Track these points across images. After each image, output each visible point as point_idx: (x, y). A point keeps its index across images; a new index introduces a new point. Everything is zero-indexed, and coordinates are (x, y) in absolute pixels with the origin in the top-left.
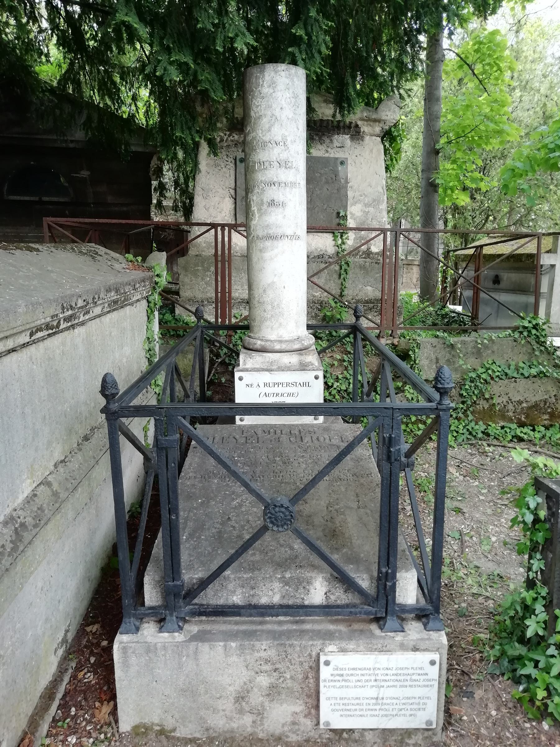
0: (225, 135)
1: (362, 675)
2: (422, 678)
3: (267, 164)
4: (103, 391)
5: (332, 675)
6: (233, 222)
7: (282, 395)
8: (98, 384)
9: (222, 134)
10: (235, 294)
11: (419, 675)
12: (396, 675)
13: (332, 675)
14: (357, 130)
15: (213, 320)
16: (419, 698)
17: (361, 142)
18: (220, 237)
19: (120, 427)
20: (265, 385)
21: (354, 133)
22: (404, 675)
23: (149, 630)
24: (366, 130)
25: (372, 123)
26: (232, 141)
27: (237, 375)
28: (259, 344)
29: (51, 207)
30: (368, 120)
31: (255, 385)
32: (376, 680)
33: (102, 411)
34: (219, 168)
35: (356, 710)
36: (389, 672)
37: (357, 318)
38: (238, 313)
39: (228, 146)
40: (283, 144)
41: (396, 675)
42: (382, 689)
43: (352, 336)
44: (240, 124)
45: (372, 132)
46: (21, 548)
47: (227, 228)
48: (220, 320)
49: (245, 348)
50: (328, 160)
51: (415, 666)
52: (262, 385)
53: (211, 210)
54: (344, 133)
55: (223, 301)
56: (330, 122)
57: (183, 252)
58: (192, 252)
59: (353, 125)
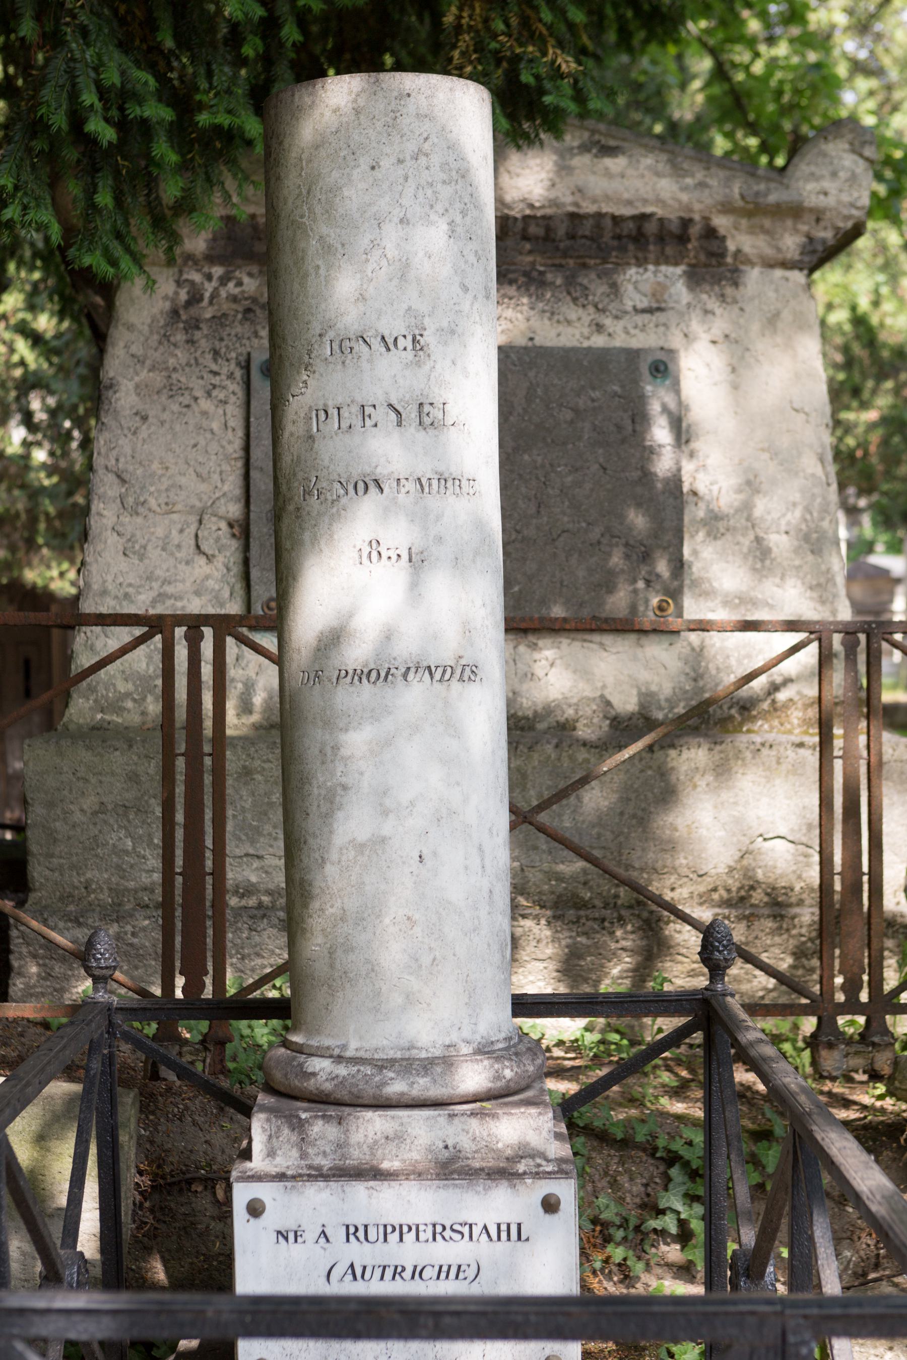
0: (209, 277)
3: (351, 415)
6: (234, 608)
7: (418, 1273)
9: (197, 277)
14: (714, 246)
17: (729, 291)
18: (181, 653)
20: (351, 1232)
21: (702, 257)
24: (747, 249)
25: (767, 223)
26: (234, 299)
27: (241, 1194)
30: (753, 211)
31: (311, 1234)
34: (186, 400)
38: (250, 963)
39: (220, 320)
40: (408, 343)
43: (698, 1037)
44: (262, 246)
45: (769, 251)
47: (208, 632)
48: (862, 739)
49: (271, 1089)
50: (600, 360)
53: (154, 553)
54: (663, 259)
55: (194, 911)
56: (608, 223)
58: (81, 709)
59: (695, 231)
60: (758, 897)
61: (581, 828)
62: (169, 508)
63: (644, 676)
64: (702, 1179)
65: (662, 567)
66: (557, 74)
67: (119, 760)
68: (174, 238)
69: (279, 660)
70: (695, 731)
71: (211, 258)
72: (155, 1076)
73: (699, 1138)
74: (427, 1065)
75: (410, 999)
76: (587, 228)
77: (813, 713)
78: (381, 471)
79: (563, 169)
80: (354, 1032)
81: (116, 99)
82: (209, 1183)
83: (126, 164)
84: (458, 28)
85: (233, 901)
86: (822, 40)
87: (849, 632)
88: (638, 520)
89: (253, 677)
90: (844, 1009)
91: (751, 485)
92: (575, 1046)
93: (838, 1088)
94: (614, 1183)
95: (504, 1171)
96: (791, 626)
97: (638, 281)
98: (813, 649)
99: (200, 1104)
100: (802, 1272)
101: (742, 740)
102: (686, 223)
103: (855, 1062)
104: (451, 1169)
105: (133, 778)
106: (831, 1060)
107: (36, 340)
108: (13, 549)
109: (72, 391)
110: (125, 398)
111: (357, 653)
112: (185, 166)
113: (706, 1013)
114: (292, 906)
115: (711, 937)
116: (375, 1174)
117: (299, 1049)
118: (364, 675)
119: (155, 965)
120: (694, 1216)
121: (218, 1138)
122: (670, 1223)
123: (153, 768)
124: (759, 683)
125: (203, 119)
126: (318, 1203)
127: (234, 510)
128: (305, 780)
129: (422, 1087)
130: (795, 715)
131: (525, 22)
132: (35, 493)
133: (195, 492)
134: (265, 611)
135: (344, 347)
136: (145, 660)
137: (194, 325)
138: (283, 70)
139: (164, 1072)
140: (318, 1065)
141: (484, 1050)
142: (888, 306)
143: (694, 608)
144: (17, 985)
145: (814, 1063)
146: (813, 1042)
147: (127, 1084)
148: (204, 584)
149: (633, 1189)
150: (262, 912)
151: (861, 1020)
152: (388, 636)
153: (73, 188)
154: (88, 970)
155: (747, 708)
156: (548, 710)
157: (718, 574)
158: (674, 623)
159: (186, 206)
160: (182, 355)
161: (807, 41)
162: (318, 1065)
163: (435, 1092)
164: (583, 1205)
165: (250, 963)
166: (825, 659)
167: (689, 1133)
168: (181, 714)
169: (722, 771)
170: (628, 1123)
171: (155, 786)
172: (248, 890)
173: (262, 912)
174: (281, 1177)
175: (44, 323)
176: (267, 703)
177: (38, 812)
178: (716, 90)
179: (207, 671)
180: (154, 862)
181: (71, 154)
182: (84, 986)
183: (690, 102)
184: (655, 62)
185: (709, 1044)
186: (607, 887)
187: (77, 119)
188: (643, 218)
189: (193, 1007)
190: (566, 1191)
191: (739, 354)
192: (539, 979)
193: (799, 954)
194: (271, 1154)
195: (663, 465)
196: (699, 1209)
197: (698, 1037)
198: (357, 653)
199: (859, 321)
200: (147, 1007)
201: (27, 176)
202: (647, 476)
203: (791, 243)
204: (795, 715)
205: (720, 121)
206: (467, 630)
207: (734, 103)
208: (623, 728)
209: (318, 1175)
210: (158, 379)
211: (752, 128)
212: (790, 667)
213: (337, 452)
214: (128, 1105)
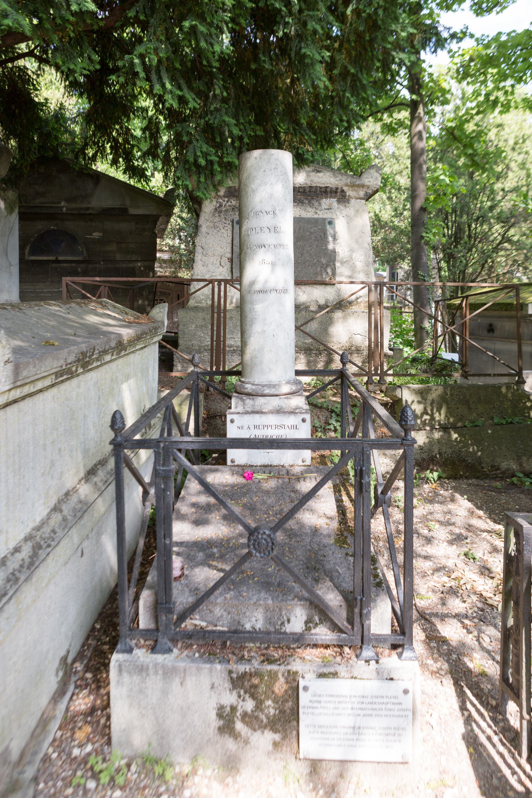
1: (339, 702)
2: (397, 707)
3: (258, 230)
4: (113, 426)
5: (310, 701)
6: (229, 278)
8: (108, 420)
10: (229, 342)
11: (393, 704)
12: (372, 703)
13: (310, 701)
15: (327, 491)
16: (395, 728)
18: (216, 289)
19: (125, 458)
20: (255, 427)
22: (379, 703)
23: (141, 655)
27: (229, 417)
28: (249, 387)
29: (65, 265)
30: (353, 186)
31: (246, 427)
32: (352, 709)
33: (111, 443)
35: (334, 739)
36: (365, 700)
37: (344, 364)
38: (232, 362)
39: (227, 211)
41: (372, 703)
42: (358, 718)
44: (236, 193)
46: (37, 564)
47: (223, 283)
49: (236, 392)
51: (389, 695)
52: (252, 427)
53: (210, 266)
54: (331, 197)
55: (218, 350)
57: (183, 305)
58: (192, 303)
59: (339, 190)
60: (353, 348)
61: (311, 332)
62: (214, 255)
63: (326, 295)
64: (341, 416)
65: (329, 271)
66: (308, 151)
67: (201, 315)
68: (218, 191)
69: (240, 290)
70: (339, 308)
71: (225, 196)
72: (208, 390)
73: (339, 406)
74: (274, 386)
75: (270, 370)
76: (313, 190)
77: (367, 304)
78: (265, 243)
79: (308, 176)
80: (255, 379)
81: (205, 155)
82: (221, 416)
83: (208, 171)
84: (285, 140)
85: (227, 349)
86: (368, 150)
87: (376, 284)
88: (324, 261)
89: (234, 295)
90: (374, 375)
91: (352, 250)
92: (309, 384)
93: (372, 395)
94: (318, 417)
95: (293, 412)
96: (362, 283)
97: (325, 202)
98: (367, 288)
99: (219, 397)
100: (366, 434)
101: (349, 311)
102: (337, 189)
103: (377, 388)
104: (279, 411)
105: (204, 319)
106: (371, 387)
107: (182, 219)
108: (176, 268)
109: (191, 230)
110: (204, 229)
111: (258, 287)
112: (221, 172)
113: (342, 375)
114: (242, 350)
115: (342, 357)
116: (262, 413)
117: (243, 382)
118: (260, 292)
119: (209, 364)
120: (337, 425)
121: (223, 406)
122: (332, 427)
123: (209, 317)
124: (353, 297)
125: (225, 160)
126: (248, 420)
127: (229, 256)
128: (246, 317)
129: (273, 391)
130: (362, 305)
131: (301, 140)
132: (181, 255)
133: (219, 251)
134: (236, 279)
135: (256, 214)
136: (207, 290)
137: (220, 212)
138: (244, 149)
139: (211, 389)
140: (247, 386)
141: (288, 382)
142: (383, 212)
143: (338, 279)
144: (175, 368)
145: (367, 388)
146: (367, 383)
147: (201, 392)
148: (222, 272)
149: (323, 419)
150: (234, 351)
151: (378, 378)
152: (266, 282)
153: (195, 177)
154: (193, 364)
155: (350, 303)
156: (303, 304)
157: (342, 272)
158: (334, 282)
159: (220, 183)
160: (217, 219)
161: (365, 150)
162: (247, 386)
163: (276, 393)
164: (312, 422)
165: (232, 362)
166: (370, 291)
167: (336, 405)
168: (216, 304)
169: (345, 318)
170: (322, 403)
171: (209, 321)
172: (231, 346)
173: (234, 351)
174: (238, 413)
175: (184, 215)
176: (237, 302)
177: (181, 327)
178: (343, 161)
179: (222, 294)
180: (209, 339)
181: (194, 169)
182: (191, 369)
183: (337, 164)
184: (329, 154)
185: (342, 382)
186: (316, 345)
187: (196, 161)
188: (327, 187)
189: (218, 373)
190: (308, 417)
191: (349, 219)
192: (301, 366)
193: (363, 362)
194: (236, 407)
195: (330, 247)
196: (339, 424)
197: (339, 381)
198: (258, 287)
199: (376, 215)
200: (205, 373)
201: (184, 174)
202: (327, 249)
203: (362, 193)
204: (362, 305)
205: (344, 168)
206: (285, 281)
207: (347, 165)
208: (321, 308)
209: (247, 413)
210: (212, 225)
211: (351, 170)
212: (361, 293)
213: (254, 238)
214: (201, 396)
